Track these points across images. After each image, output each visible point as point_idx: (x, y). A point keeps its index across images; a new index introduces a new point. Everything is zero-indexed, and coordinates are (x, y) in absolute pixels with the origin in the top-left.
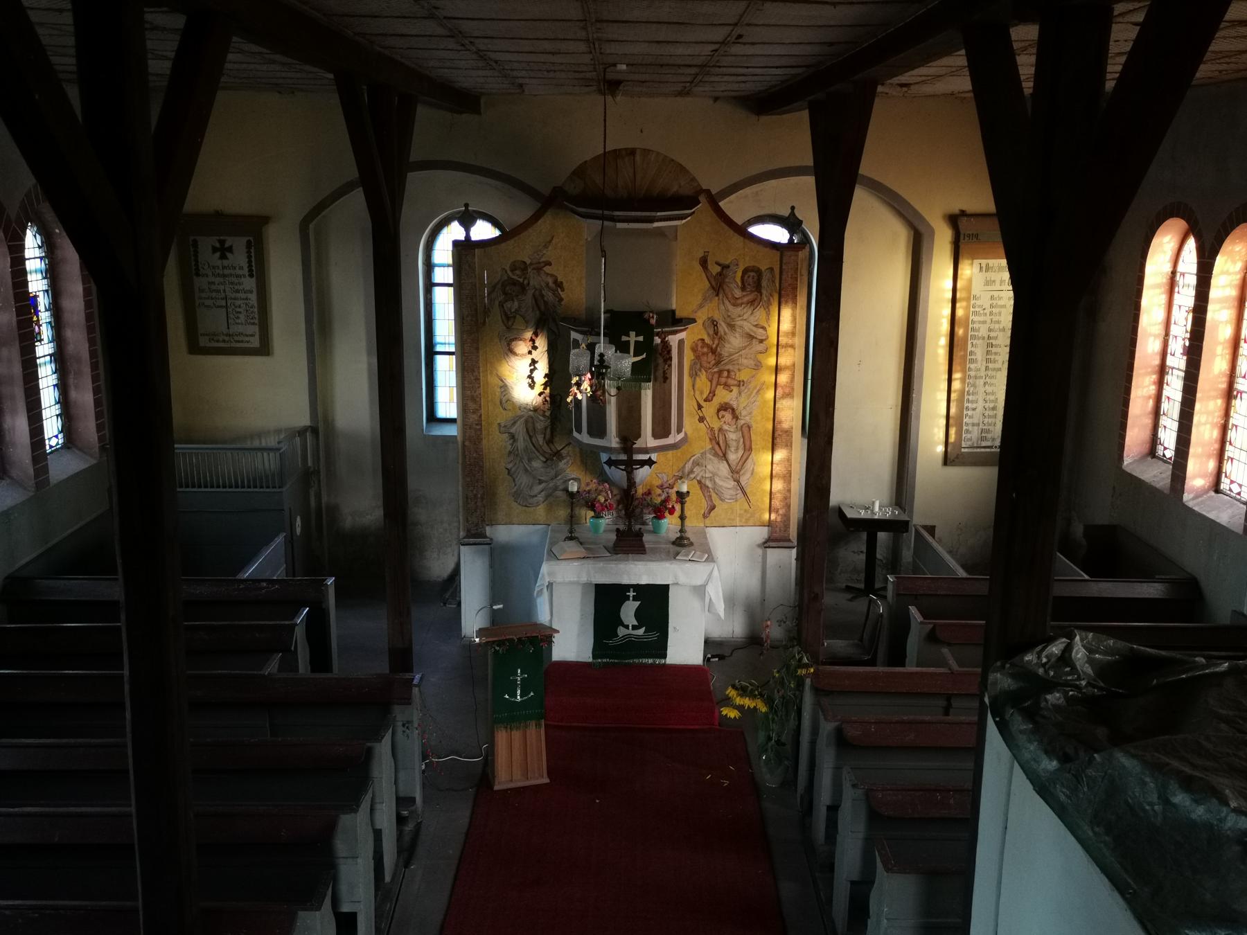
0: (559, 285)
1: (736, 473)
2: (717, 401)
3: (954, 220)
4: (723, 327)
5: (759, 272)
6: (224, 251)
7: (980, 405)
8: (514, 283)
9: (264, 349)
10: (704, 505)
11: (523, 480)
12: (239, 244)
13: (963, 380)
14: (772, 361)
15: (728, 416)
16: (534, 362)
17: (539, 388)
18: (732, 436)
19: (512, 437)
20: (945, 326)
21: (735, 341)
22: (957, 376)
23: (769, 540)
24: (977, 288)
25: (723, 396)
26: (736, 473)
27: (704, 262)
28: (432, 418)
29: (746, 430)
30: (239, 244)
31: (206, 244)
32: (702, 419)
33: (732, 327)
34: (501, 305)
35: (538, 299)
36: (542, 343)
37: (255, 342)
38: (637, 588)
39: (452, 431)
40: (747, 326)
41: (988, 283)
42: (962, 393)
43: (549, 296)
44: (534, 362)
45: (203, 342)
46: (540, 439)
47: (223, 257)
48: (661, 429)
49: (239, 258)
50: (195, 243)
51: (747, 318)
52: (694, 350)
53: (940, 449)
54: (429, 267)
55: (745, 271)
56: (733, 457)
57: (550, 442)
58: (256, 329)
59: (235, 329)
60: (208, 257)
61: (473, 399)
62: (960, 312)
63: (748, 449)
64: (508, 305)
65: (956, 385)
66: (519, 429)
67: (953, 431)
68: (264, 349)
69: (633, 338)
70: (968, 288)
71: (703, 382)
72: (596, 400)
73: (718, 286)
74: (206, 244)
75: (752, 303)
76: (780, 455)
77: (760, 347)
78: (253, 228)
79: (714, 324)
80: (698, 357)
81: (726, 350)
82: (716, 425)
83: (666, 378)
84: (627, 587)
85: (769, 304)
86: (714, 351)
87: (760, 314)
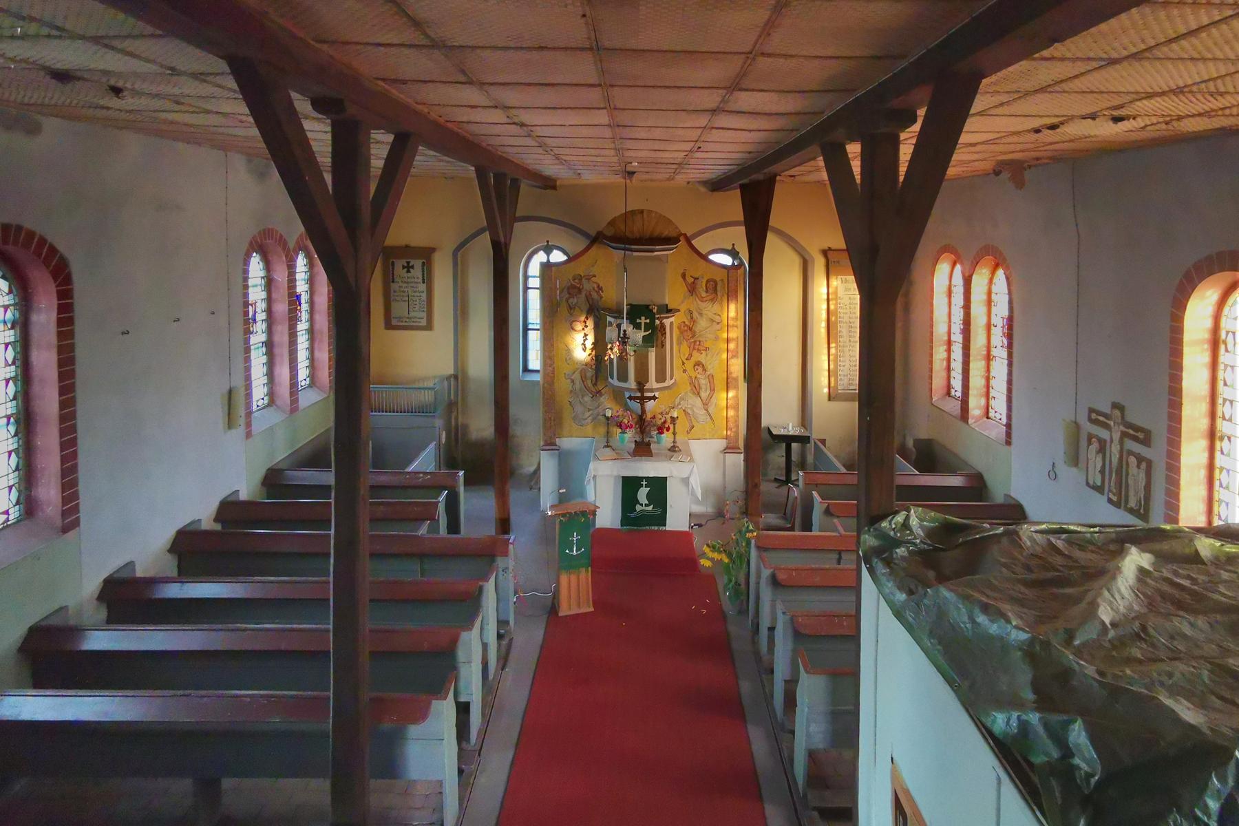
0: (600, 289)
1: (706, 405)
2: (693, 360)
3: (825, 253)
4: (695, 315)
5: (716, 283)
6: (409, 268)
7: (847, 363)
8: (575, 287)
9: (429, 327)
10: (688, 426)
11: (579, 409)
12: (417, 263)
13: (836, 348)
14: (725, 335)
15: (700, 369)
16: (586, 335)
17: (588, 351)
18: (703, 382)
19: (573, 381)
20: (824, 316)
21: (702, 324)
22: (833, 345)
23: (727, 448)
24: (841, 293)
25: (696, 357)
26: (706, 405)
27: (684, 276)
28: (526, 369)
29: (711, 378)
30: (417, 263)
31: (399, 264)
32: (685, 371)
33: (701, 314)
34: (567, 300)
35: (588, 297)
36: (590, 323)
37: (424, 323)
38: (647, 479)
39: (537, 378)
40: (710, 315)
41: (846, 290)
42: (836, 356)
43: (595, 295)
44: (586, 335)
45: (394, 322)
46: (589, 383)
47: (408, 271)
48: (661, 377)
49: (417, 272)
50: (393, 264)
51: (710, 309)
52: (679, 328)
53: (826, 390)
54: (526, 277)
55: (708, 281)
56: (704, 395)
57: (595, 385)
58: (424, 315)
59: (412, 314)
60: (399, 271)
61: (550, 358)
62: (832, 307)
63: (713, 390)
64: (571, 300)
65: (833, 351)
66: (577, 376)
67: (832, 379)
68: (429, 327)
69: (643, 320)
70: (836, 293)
71: (685, 349)
72: (622, 359)
73: (692, 289)
74: (399, 264)
75: (712, 300)
76: (731, 394)
77: (718, 327)
78: (426, 254)
79: (691, 313)
80: (682, 332)
81: (697, 329)
82: (693, 374)
83: (663, 346)
84: (641, 479)
85: (721, 303)
86: (690, 329)
87: (716, 307)
